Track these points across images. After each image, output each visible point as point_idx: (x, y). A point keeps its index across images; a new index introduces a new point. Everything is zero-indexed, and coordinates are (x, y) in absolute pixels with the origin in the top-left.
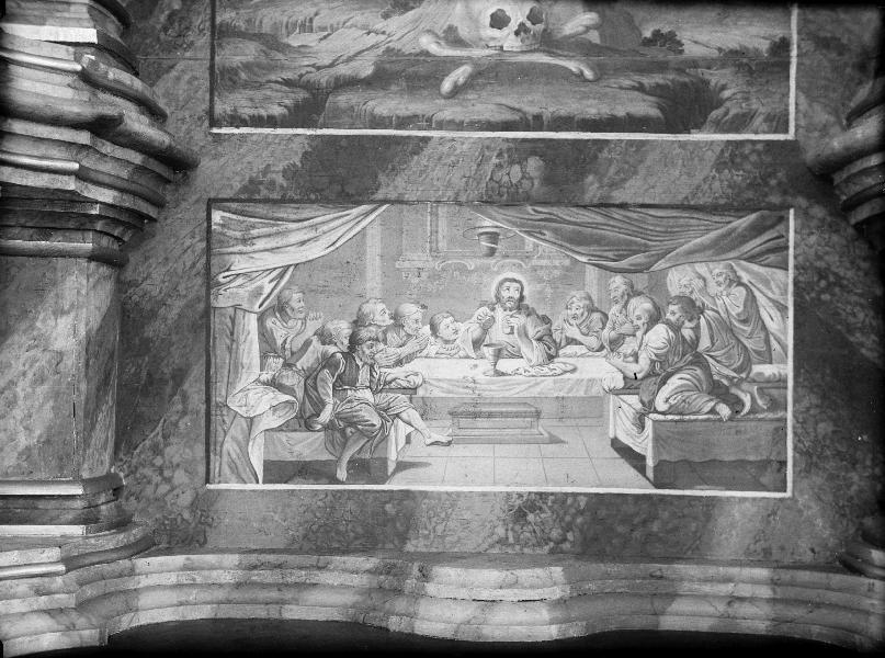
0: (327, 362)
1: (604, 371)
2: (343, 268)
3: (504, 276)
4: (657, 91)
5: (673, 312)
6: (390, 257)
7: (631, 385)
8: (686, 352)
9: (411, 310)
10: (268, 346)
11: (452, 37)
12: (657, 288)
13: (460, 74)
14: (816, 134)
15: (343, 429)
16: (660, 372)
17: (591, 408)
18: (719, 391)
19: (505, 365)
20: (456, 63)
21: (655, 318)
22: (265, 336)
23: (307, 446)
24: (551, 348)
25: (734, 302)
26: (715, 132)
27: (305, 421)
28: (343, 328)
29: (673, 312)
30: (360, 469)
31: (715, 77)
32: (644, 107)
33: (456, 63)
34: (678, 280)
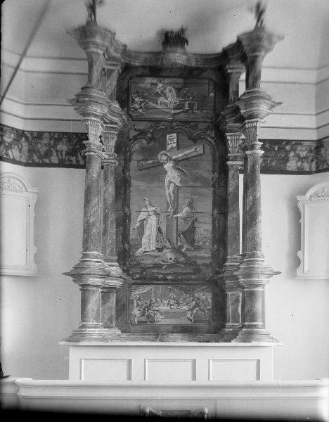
0: (147, 307)
1: (186, 308)
2: (149, 293)
3: (172, 295)
4: (194, 269)
5: (196, 299)
6: (155, 292)
7: (190, 310)
8: (197, 305)
9: (158, 300)
10: (138, 305)
11: (164, 261)
12: (194, 296)
13: (165, 266)
14: (127, 285)
15: (149, 316)
16: (194, 308)
17: (184, 313)
18: (202, 310)
19: (172, 307)
20: (164, 265)
21: (193, 300)
22: (137, 303)
23: (143, 319)
24: (178, 304)
25: (204, 297)
26: (191, 341)
27: (143, 315)
28: (149, 302)
29: (196, 299)
30: (151, 322)
31: (201, 267)
32: (192, 271)
33: (164, 265)
34: (196, 295)
